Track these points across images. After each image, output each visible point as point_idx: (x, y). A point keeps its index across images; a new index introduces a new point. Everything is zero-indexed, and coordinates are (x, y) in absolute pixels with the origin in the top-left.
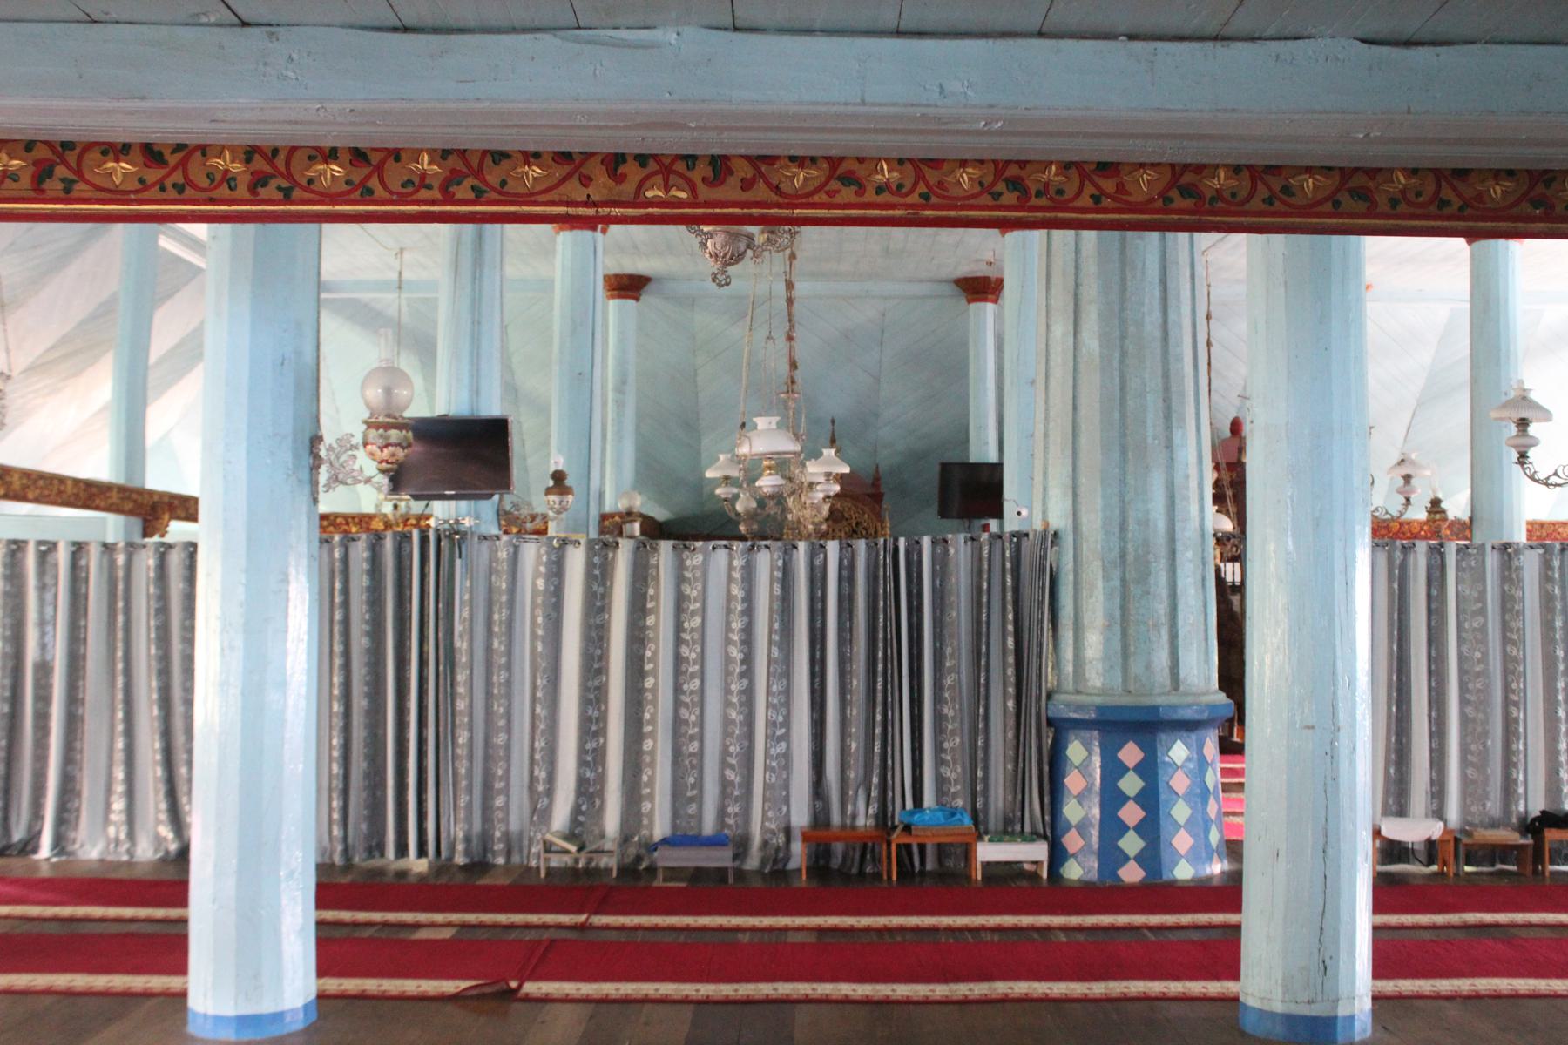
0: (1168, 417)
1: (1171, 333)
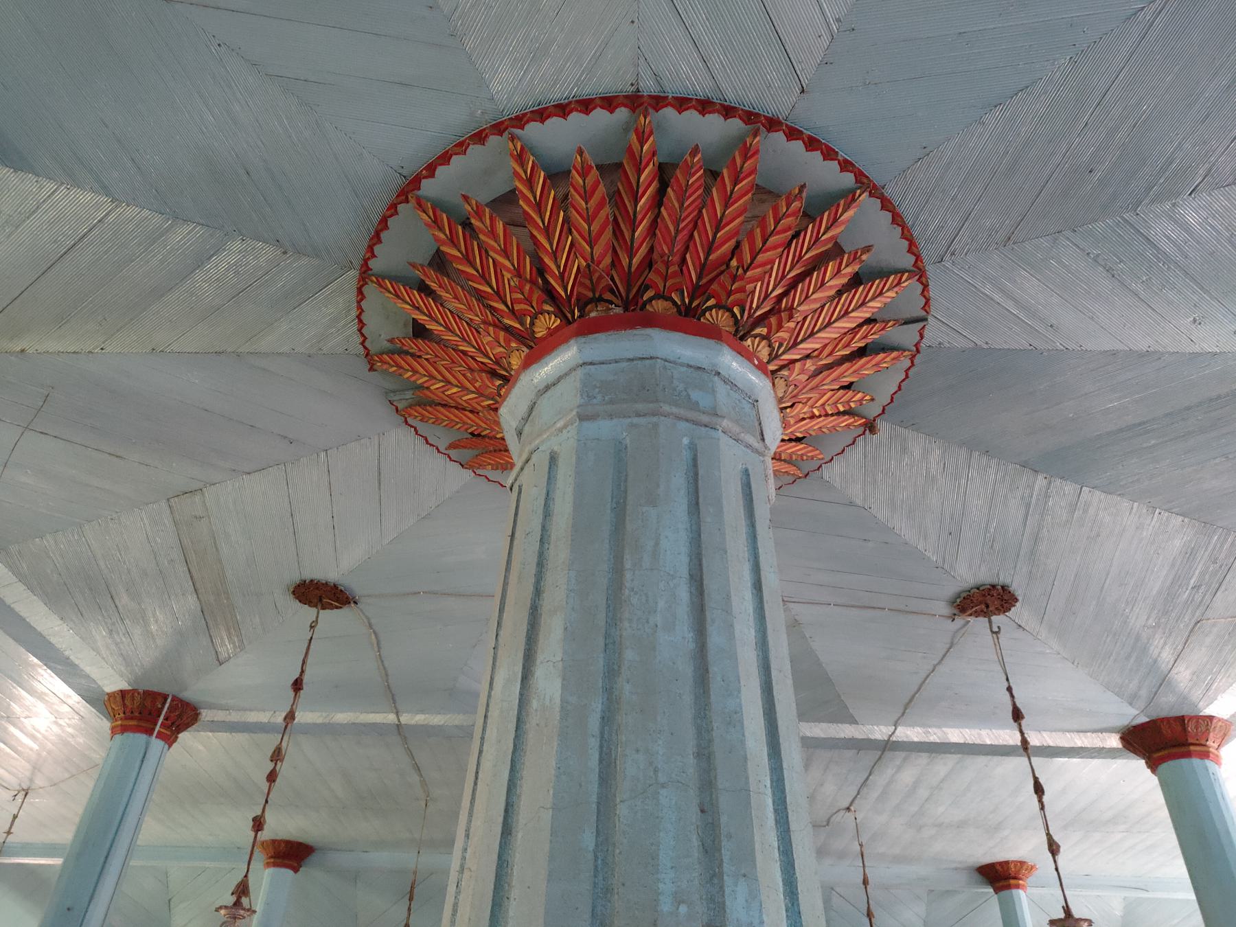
0: (711, 849)
1: (714, 669)
